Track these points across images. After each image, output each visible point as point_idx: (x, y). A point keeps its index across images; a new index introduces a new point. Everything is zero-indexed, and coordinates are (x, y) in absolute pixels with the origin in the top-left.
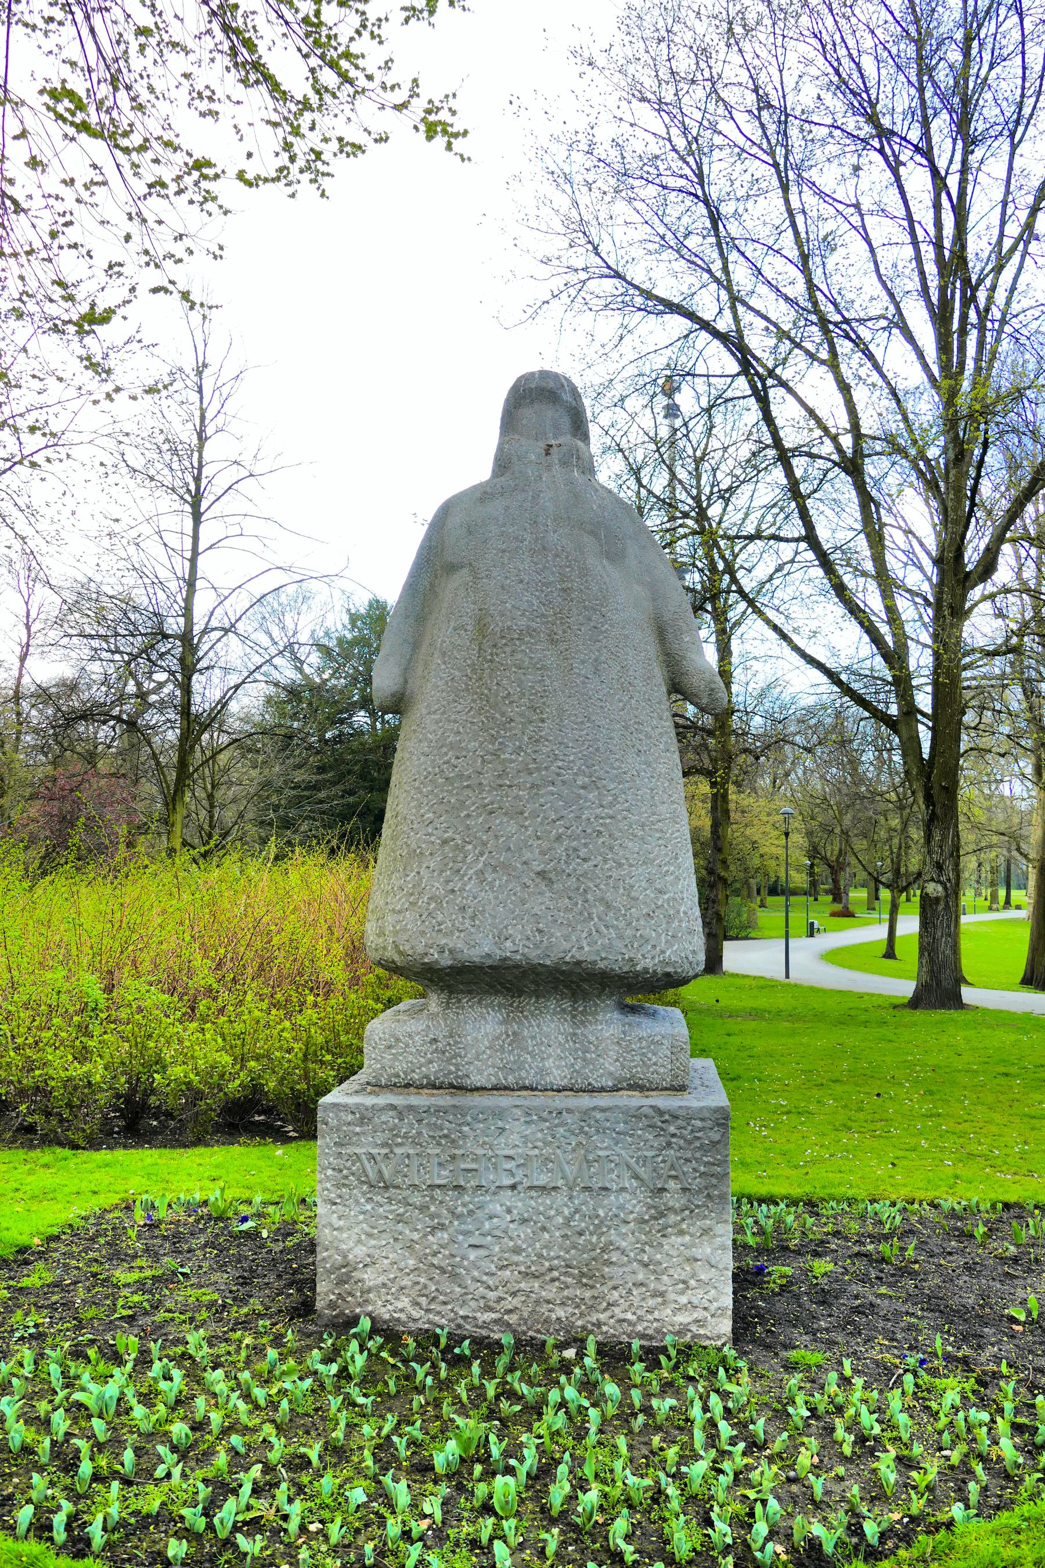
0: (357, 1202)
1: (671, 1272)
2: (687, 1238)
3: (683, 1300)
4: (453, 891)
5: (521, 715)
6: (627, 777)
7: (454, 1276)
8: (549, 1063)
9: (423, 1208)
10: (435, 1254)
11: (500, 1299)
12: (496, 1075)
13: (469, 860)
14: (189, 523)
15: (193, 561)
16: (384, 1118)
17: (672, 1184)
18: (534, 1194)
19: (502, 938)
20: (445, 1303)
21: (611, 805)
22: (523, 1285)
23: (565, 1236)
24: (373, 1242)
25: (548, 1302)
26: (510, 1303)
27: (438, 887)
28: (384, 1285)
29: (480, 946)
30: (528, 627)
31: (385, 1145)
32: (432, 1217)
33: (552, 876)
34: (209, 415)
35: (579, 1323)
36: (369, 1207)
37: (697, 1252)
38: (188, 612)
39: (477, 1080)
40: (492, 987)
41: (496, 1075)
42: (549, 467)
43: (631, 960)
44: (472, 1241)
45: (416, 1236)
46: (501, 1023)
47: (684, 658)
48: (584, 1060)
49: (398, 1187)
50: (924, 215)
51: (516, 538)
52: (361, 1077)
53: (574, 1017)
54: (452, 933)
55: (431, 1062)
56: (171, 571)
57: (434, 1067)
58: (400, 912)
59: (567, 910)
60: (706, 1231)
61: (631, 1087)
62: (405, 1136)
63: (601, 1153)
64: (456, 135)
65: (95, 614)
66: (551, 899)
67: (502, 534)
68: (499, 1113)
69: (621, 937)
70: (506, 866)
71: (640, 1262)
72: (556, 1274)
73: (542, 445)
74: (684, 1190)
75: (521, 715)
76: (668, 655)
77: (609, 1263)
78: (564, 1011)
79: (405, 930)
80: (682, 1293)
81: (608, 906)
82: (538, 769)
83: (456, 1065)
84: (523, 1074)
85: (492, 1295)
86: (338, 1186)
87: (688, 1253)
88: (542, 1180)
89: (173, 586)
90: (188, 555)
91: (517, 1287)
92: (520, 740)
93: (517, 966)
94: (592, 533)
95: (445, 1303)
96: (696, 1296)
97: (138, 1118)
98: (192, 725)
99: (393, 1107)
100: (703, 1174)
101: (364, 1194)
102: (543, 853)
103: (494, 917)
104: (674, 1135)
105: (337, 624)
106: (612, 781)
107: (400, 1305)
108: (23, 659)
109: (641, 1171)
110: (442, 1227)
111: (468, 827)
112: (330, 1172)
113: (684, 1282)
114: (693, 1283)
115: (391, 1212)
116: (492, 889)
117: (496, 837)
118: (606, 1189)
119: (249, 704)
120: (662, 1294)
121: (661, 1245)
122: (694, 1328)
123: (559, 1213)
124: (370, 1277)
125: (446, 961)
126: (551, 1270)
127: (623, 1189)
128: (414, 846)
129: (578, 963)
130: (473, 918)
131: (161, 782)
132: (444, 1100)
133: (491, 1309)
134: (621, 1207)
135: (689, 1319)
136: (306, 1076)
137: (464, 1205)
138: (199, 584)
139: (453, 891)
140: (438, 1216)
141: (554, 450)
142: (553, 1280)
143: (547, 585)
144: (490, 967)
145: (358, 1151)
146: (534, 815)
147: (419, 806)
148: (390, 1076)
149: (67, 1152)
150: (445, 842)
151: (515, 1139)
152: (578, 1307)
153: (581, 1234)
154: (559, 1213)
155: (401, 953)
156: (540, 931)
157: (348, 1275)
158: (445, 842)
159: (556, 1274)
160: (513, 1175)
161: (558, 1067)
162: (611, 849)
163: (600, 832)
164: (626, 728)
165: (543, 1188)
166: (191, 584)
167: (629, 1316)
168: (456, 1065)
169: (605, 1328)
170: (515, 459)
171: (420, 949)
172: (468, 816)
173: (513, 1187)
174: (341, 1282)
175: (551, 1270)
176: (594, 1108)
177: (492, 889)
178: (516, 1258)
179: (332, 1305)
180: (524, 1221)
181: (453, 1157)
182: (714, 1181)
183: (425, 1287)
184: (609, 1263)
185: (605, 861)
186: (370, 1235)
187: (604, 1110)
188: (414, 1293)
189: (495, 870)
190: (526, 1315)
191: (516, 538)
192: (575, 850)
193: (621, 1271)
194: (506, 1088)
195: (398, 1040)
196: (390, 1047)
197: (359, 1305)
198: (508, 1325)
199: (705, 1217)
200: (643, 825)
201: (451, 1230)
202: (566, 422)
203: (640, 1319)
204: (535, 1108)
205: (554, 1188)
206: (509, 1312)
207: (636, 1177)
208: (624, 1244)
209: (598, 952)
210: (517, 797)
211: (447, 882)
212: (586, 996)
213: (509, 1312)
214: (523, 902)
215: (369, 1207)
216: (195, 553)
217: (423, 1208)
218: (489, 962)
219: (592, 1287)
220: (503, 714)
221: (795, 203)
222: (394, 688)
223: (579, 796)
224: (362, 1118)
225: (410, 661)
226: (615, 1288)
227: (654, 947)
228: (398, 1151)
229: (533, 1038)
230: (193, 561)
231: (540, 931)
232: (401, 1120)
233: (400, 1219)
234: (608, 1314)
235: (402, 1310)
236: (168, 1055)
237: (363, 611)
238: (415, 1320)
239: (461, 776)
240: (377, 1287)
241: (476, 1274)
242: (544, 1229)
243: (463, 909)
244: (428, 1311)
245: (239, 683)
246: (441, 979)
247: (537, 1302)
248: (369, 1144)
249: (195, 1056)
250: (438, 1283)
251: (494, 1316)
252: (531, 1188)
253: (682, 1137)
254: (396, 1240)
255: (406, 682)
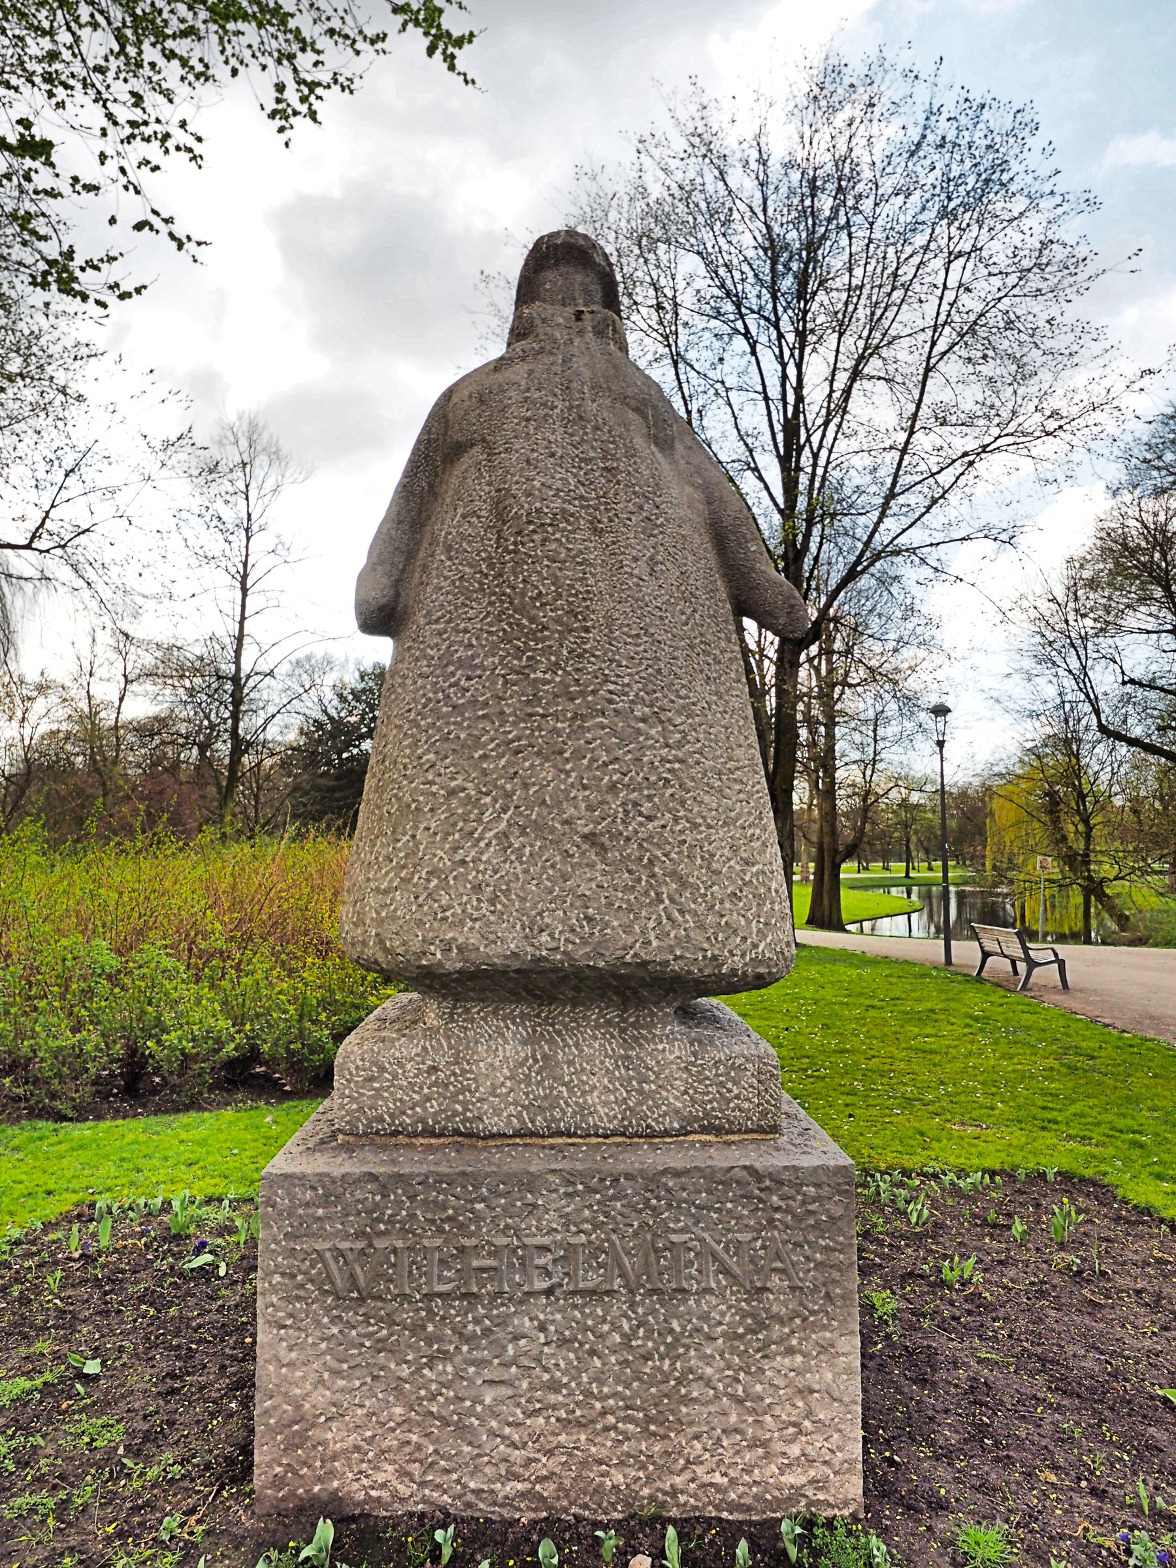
0: (318, 1323)
1: (777, 1410)
2: (799, 1359)
3: (795, 1450)
4: (463, 862)
5: (558, 621)
6: (697, 709)
7: (462, 1431)
8: (593, 1098)
9: (417, 1328)
10: (433, 1397)
11: (530, 1461)
12: (519, 1116)
13: (486, 818)
14: (238, 594)
15: (241, 623)
16: (359, 1194)
17: (776, 1281)
18: (579, 1301)
19: (534, 928)
20: (447, 1471)
21: (679, 745)
22: (562, 1438)
23: (625, 1363)
24: (341, 1383)
25: (600, 1462)
26: (546, 1465)
27: (442, 857)
28: (357, 1448)
29: (505, 942)
30: (563, 510)
31: (360, 1235)
32: (429, 1342)
33: (605, 839)
34: (253, 517)
35: (646, 1492)
36: (335, 1330)
37: (812, 1379)
38: (237, 662)
39: (492, 1123)
40: (513, 993)
41: (519, 1116)
42: (581, 333)
43: (715, 958)
44: (487, 1374)
45: (405, 1371)
46: (524, 1043)
47: (753, 569)
48: (641, 1092)
49: (379, 1298)
50: (774, 392)
51: (544, 404)
52: (334, 1107)
53: (623, 1031)
54: (462, 923)
55: (429, 1099)
56: (226, 629)
57: (433, 1107)
58: (386, 892)
59: (628, 889)
60: (824, 1349)
61: (704, 1130)
62: (391, 1221)
63: (674, 1238)
64: (459, 42)
65: (171, 666)
66: (604, 873)
67: (526, 399)
68: (530, 1183)
69: (701, 926)
70: (539, 827)
71: (733, 1397)
72: (611, 1419)
73: (570, 310)
74: (793, 1289)
75: (558, 621)
76: (730, 567)
77: (687, 1400)
78: (609, 1023)
79: (393, 917)
80: (792, 1440)
81: (683, 882)
82: (582, 693)
83: (464, 1104)
84: (557, 1114)
85: (517, 1455)
86: (288, 1300)
87: (800, 1382)
88: (592, 1279)
89: (227, 641)
90: (238, 618)
91: (555, 1441)
92: (558, 654)
93: (555, 970)
94: (636, 410)
95: (447, 1471)
96: (817, 1445)
97: (135, 1084)
98: (240, 746)
99: (372, 1177)
100: (819, 1265)
101: (328, 1310)
102: (591, 808)
103: (523, 900)
104: (777, 1209)
105: (352, 680)
106: (679, 713)
107: (380, 1478)
108: (121, 699)
109: (732, 1262)
110: (446, 1356)
111: (484, 773)
112: (277, 1278)
113: (795, 1424)
114: (807, 1423)
115: (369, 1336)
116: (519, 858)
117: (526, 786)
118: (682, 1290)
119: (284, 732)
120: (764, 1444)
121: (762, 1371)
122: (809, 1493)
123: (615, 1328)
124: (335, 1437)
125: (454, 964)
126: (604, 1413)
127: (708, 1290)
128: (407, 798)
129: (645, 964)
130: (493, 901)
131: (219, 786)
132: (450, 1162)
133: (517, 1477)
134: (705, 1317)
135: (803, 1480)
136: (301, 1035)
137: (476, 1321)
138: (246, 640)
139: (463, 862)
140: (439, 1339)
141: (587, 316)
142: (606, 1429)
143: (589, 461)
144: (518, 971)
145: (321, 1245)
146: (578, 755)
147: (415, 745)
148: (370, 1121)
149: (45, 1126)
150: (452, 793)
151: (551, 1219)
152: (643, 1467)
153: (647, 1358)
154: (615, 1328)
155: (387, 951)
156: (589, 919)
157: (302, 1435)
158: (452, 793)
159: (611, 1419)
160: (549, 1275)
161: (606, 1104)
162: (683, 803)
163: (667, 781)
164: (692, 647)
165: (593, 1292)
166: (240, 639)
167: (718, 1478)
168: (464, 1104)
169: (682, 1498)
170: (538, 322)
171: (416, 945)
172: (484, 757)
173: (549, 1292)
174: (291, 1447)
175: (604, 1413)
176: (664, 1172)
177: (519, 858)
178: (553, 1398)
179: (278, 1482)
180: (564, 1342)
181: (462, 1250)
182: (836, 1275)
183: (419, 1447)
184: (687, 1400)
185: (676, 820)
186: (336, 1373)
187: (677, 1174)
188: (401, 1458)
189: (523, 833)
190: (567, 1483)
191: (544, 404)
192: (636, 804)
193: (705, 1410)
194: (533, 1134)
195: (383, 1069)
196: (371, 1079)
197: (319, 1480)
198: (543, 1499)
199: (824, 1328)
200: (720, 773)
201: (458, 1359)
202: (596, 289)
203: (733, 1482)
204: (581, 1174)
205: (608, 1293)
206: (542, 1479)
207: (727, 1272)
208: (709, 1371)
209: (671, 949)
210: (555, 731)
211: (455, 849)
212: (640, 1003)
213: (542, 1479)
214: (565, 878)
215: (335, 1330)
216: (243, 618)
217: (417, 1328)
218: (516, 965)
219: (665, 1437)
220: (532, 620)
221: (683, 378)
222: (383, 601)
223: (639, 732)
224: (327, 1196)
225: (403, 571)
226: (697, 1437)
227: (744, 939)
228: (380, 1244)
229: (571, 1063)
230: (241, 623)
231: (589, 919)
232: (385, 1196)
233: (381, 1346)
234: (687, 1475)
235: (383, 1486)
236: (168, 1017)
237: (370, 671)
238: (403, 1500)
239: (473, 702)
240: (345, 1451)
241: (494, 1424)
242: (593, 1353)
243: (477, 888)
244: (422, 1484)
245: (280, 722)
246: (444, 986)
247: (584, 1464)
248: (336, 1234)
249: (196, 1018)
250: (436, 1441)
251: (520, 1486)
252: (574, 1293)
253: (788, 1211)
254: (375, 1378)
255: (397, 595)
